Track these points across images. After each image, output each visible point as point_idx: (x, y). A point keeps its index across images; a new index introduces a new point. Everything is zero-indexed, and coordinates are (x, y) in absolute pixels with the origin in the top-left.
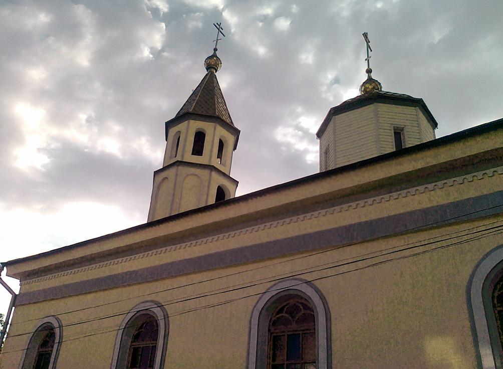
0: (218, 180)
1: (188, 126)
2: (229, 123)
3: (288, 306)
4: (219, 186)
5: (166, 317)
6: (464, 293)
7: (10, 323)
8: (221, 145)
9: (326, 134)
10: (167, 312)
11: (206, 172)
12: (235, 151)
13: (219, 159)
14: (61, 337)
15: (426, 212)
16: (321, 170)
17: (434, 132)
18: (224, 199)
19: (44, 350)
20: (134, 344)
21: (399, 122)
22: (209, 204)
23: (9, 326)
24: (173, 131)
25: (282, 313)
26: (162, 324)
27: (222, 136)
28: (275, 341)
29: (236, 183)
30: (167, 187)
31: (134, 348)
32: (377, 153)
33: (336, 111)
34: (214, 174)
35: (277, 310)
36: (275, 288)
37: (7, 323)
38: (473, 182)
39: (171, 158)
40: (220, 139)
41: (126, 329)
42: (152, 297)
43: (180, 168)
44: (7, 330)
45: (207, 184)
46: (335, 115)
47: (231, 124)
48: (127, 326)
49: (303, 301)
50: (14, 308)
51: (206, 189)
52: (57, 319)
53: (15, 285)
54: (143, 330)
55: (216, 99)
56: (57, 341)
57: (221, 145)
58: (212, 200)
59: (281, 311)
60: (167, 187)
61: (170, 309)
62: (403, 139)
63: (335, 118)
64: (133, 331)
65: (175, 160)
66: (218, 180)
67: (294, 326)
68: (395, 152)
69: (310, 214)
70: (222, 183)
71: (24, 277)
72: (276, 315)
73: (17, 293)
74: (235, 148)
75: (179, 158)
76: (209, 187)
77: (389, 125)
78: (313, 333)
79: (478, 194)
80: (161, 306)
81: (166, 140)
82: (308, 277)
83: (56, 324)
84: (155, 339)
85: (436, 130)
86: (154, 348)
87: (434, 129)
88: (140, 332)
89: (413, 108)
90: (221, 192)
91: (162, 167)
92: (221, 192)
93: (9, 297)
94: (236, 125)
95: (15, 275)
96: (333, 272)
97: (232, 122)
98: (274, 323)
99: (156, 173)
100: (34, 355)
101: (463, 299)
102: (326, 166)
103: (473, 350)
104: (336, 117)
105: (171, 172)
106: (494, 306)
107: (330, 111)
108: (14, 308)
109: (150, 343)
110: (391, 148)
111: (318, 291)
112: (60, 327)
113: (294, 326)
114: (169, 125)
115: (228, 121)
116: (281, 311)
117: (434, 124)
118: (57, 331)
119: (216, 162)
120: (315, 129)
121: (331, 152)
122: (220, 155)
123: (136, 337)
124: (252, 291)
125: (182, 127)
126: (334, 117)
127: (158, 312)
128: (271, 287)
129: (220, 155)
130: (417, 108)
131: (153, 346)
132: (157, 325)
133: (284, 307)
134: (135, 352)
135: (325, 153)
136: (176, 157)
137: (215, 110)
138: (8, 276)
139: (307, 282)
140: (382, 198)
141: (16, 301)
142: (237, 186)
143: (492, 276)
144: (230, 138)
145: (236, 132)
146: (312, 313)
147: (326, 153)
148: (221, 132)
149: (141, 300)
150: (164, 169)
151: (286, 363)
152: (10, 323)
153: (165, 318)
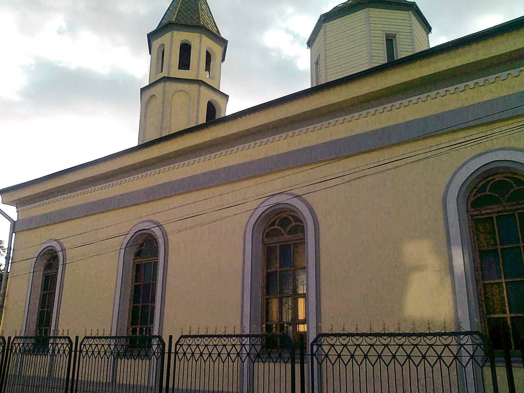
0: (207, 95)
1: (172, 37)
2: (216, 33)
3: (281, 218)
4: (209, 102)
5: (165, 235)
6: (441, 200)
7: (12, 248)
8: (209, 56)
9: (315, 45)
10: (165, 231)
11: (194, 87)
12: (224, 62)
13: (208, 72)
14: (64, 259)
15: (408, 125)
16: (312, 85)
17: (428, 38)
18: (215, 118)
19: (49, 272)
20: (136, 261)
21: (392, 30)
22: (199, 124)
23: (12, 251)
24: (156, 44)
25: (275, 225)
26: (161, 241)
27: (208, 48)
28: (269, 252)
29: (226, 97)
30: (156, 104)
31: (136, 265)
32: (368, 66)
33: (326, 18)
34: (203, 89)
35: (270, 223)
36: (264, 204)
37: (9, 249)
38: (446, 96)
39: (157, 74)
40: (207, 51)
41: (127, 248)
42: (152, 218)
43: (168, 84)
44: (11, 255)
45: (196, 100)
46: (325, 23)
47: (219, 35)
48: (128, 246)
49: (292, 213)
50: (14, 234)
51: (196, 104)
52: (61, 245)
53: (12, 211)
54: (143, 248)
55: (200, 6)
56: (61, 263)
57: (209, 56)
58: (203, 120)
59: (273, 224)
60: (156, 104)
61: (168, 228)
62: (395, 47)
63: (325, 26)
64: (135, 250)
65: (161, 76)
66: (207, 95)
67: (286, 237)
68: (387, 63)
69: (312, 126)
70: (210, 99)
71: (18, 203)
72: (269, 228)
73: (15, 220)
74: (223, 60)
75: (164, 74)
76: (198, 103)
77: (381, 32)
78: (303, 242)
79: (459, 105)
80: (159, 226)
81: (150, 54)
82: (298, 192)
83: (58, 248)
84: (156, 253)
85: (430, 35)
86: (156, 264)
87: (428, 34)
88: (142, 250)
89: (406, 12)
90: (211, 109)
91: (148, 84)
92: (211, 109)
93: (8, 224)
94: (223, 35)
95: (9, 202)
96: (323, 185)
97: (218, 31)
98: (268, 235)
99: (143, 90)
100: (40, 275)
101: (439, 206)
102: (317, 80)
103: (445, 249)
104: (327, 24)
105: (160, 87)
106: (468, 211)
107: (320, 18)
108: (14, 234)
109: (151, 260)
110: (383, 60)
111: (307, 204)
112: (63, 250)
113: (286, 237)
114: (151, 37)
115: (215, 31)
116: (273, 224)
117: (428, 29)
118: (60, 254)
119: (205, 76)
120: (307, 34)
121: (322, 63)
122: (208, 68)
123: (138, 254)
124: (245, 207)
125: (165, 39)
126: (324, 25)
127: (157, 232)
128: (262, 203)
129: (208, 68)
130: (410, 12)
131: (154, 262)
132: (157, 243)
133: (275, 221)
134: (138, 268)
135: (316, 63)
136: (161, 72)
137: (199, 18)
138: (3, 203)
139: (297, 196)
140: (368, 112)
141: (15, 227)
142: (228, 100)
143: (468, 182)
144: (216, 49)
145: (223, 43)
146: (302, 224)
147: (317, 64)
148: (207, 43)
149: (140, 220)
150: (151, 85)
151: (279, 270)
152: (12, 248)
153: (164, 237)
